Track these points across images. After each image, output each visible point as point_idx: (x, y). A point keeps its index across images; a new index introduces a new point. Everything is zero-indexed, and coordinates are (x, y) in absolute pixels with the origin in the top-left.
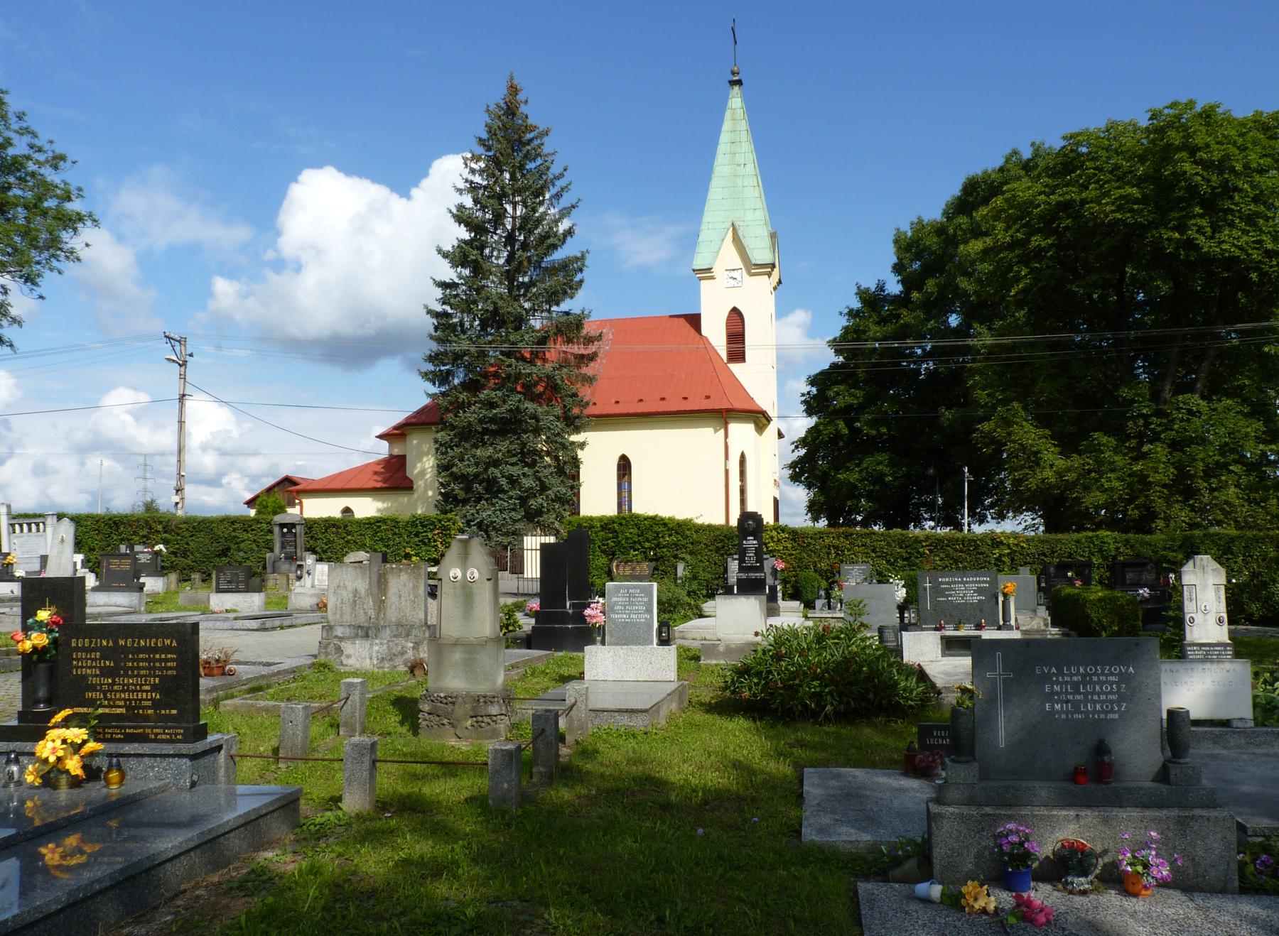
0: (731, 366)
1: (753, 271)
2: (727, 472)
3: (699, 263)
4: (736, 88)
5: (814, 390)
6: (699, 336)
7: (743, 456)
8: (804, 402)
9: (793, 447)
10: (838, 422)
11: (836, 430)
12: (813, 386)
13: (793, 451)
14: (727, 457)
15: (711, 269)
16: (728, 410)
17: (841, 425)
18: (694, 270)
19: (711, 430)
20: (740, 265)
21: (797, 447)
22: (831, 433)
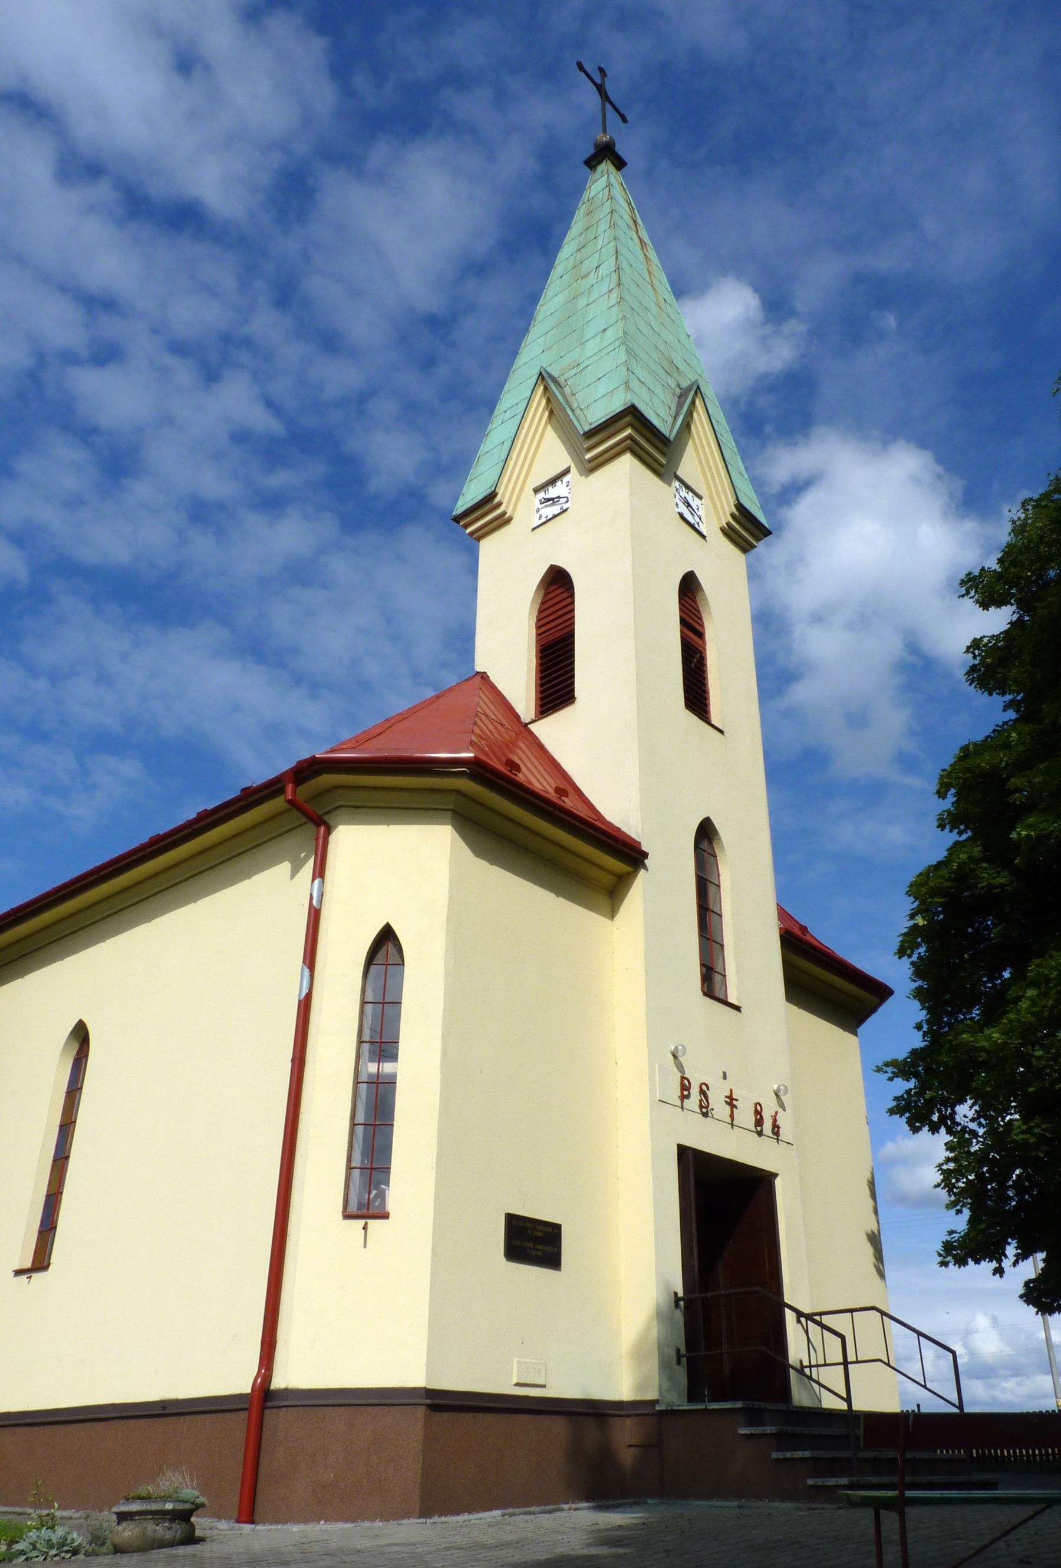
1: (588, 456)
18: (457, 519)
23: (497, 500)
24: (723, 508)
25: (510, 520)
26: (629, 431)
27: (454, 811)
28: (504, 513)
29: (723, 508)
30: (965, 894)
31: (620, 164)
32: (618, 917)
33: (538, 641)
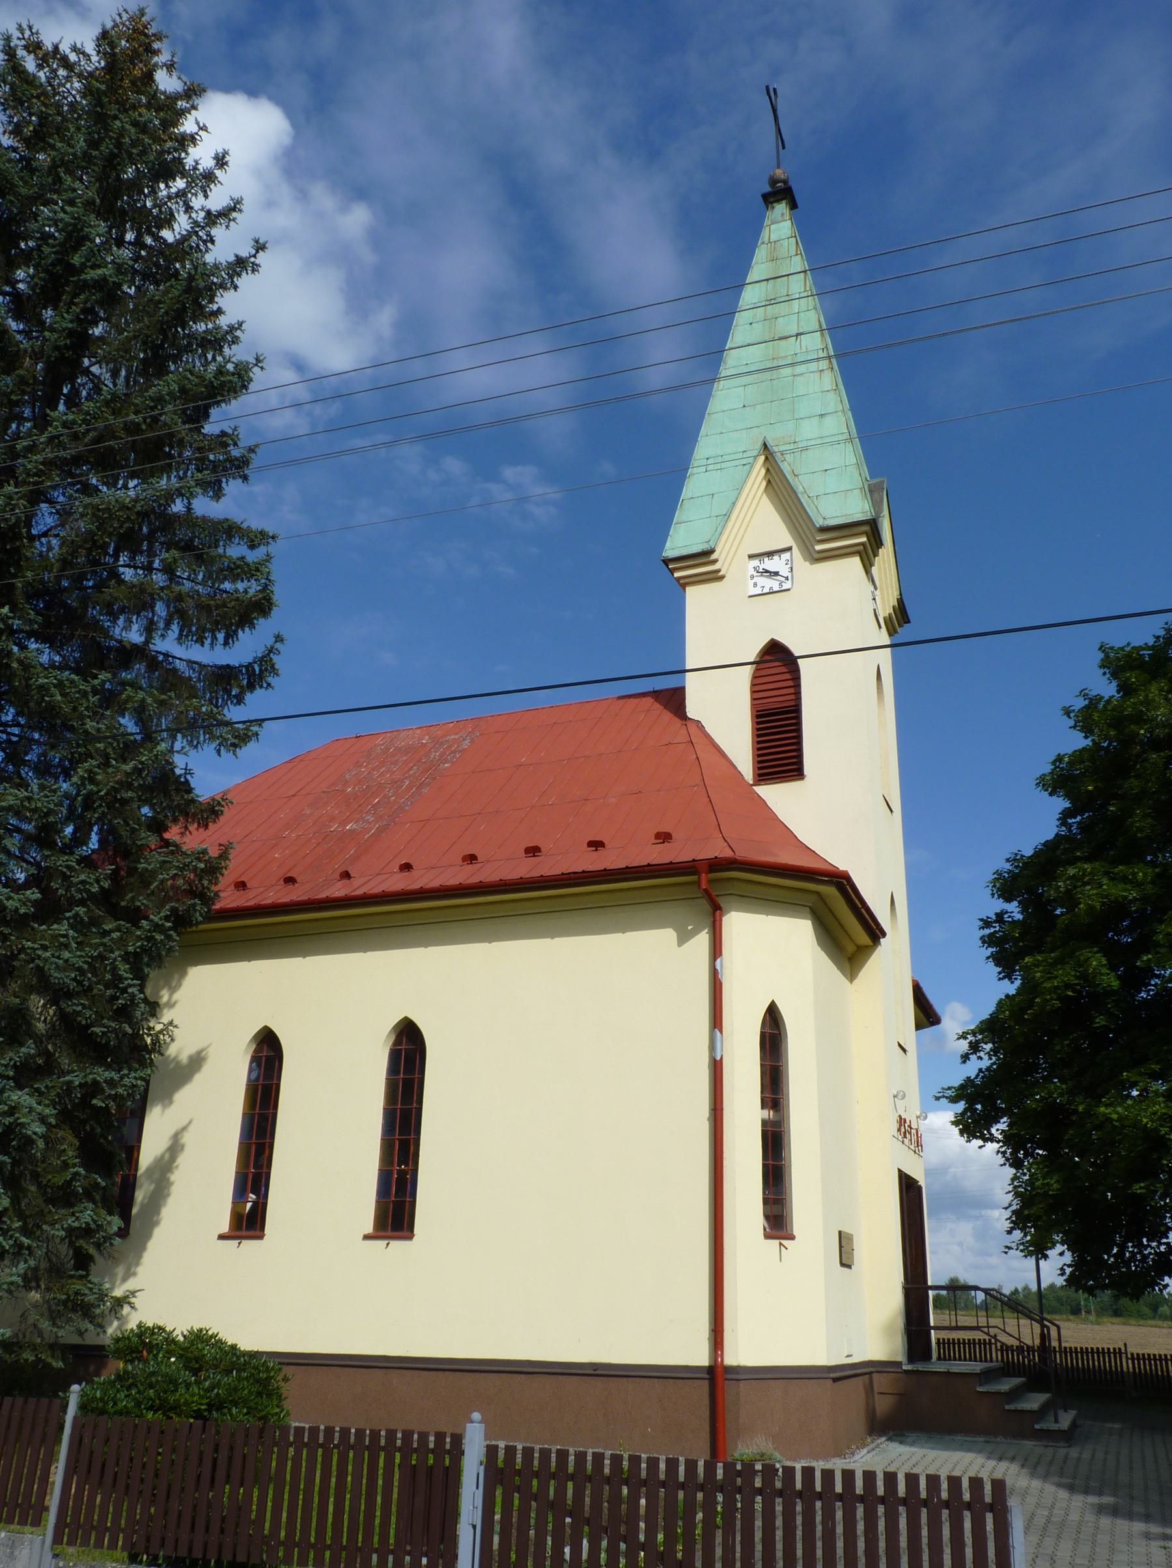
0: (765, 791)
1: (818, 547)
2: (716, 1069)
3: (679, 542)
4: (781, 208)
5: (1014, 910)
6: (678, 722)
7: (773, 1018)
8: (988, 941)
9: (964, 1046)
10: (1085, 953)
11: (1084, 977)
12: (1008, 900)
13: (965, 1058)
14: (716, 1020)
15: (712, 551)
16: (717, 865)
17: (1096, 961)
18: (666, 562)
19: (668, 935)
20: (782, 536)
21: (975, 1047)
22: (1067, 986)
23: (713, 557)
24: (889, 601)
25: (723, 577)
26: (864, 539)
27: (811, 908)
28: (719, 571)
29: (889, 601)
30: (1027, 959)
31: (793, 205)
32: (855, 982)
33: (753, 706)
